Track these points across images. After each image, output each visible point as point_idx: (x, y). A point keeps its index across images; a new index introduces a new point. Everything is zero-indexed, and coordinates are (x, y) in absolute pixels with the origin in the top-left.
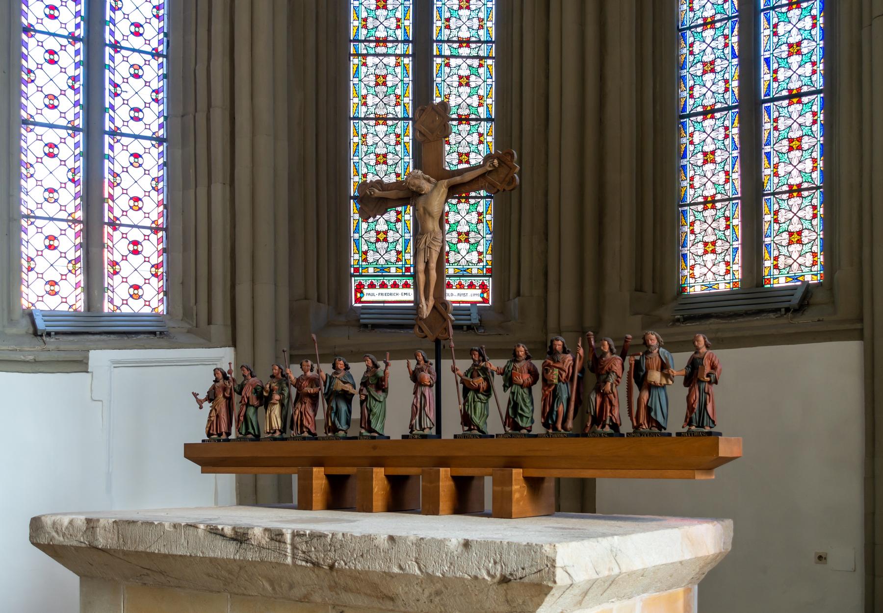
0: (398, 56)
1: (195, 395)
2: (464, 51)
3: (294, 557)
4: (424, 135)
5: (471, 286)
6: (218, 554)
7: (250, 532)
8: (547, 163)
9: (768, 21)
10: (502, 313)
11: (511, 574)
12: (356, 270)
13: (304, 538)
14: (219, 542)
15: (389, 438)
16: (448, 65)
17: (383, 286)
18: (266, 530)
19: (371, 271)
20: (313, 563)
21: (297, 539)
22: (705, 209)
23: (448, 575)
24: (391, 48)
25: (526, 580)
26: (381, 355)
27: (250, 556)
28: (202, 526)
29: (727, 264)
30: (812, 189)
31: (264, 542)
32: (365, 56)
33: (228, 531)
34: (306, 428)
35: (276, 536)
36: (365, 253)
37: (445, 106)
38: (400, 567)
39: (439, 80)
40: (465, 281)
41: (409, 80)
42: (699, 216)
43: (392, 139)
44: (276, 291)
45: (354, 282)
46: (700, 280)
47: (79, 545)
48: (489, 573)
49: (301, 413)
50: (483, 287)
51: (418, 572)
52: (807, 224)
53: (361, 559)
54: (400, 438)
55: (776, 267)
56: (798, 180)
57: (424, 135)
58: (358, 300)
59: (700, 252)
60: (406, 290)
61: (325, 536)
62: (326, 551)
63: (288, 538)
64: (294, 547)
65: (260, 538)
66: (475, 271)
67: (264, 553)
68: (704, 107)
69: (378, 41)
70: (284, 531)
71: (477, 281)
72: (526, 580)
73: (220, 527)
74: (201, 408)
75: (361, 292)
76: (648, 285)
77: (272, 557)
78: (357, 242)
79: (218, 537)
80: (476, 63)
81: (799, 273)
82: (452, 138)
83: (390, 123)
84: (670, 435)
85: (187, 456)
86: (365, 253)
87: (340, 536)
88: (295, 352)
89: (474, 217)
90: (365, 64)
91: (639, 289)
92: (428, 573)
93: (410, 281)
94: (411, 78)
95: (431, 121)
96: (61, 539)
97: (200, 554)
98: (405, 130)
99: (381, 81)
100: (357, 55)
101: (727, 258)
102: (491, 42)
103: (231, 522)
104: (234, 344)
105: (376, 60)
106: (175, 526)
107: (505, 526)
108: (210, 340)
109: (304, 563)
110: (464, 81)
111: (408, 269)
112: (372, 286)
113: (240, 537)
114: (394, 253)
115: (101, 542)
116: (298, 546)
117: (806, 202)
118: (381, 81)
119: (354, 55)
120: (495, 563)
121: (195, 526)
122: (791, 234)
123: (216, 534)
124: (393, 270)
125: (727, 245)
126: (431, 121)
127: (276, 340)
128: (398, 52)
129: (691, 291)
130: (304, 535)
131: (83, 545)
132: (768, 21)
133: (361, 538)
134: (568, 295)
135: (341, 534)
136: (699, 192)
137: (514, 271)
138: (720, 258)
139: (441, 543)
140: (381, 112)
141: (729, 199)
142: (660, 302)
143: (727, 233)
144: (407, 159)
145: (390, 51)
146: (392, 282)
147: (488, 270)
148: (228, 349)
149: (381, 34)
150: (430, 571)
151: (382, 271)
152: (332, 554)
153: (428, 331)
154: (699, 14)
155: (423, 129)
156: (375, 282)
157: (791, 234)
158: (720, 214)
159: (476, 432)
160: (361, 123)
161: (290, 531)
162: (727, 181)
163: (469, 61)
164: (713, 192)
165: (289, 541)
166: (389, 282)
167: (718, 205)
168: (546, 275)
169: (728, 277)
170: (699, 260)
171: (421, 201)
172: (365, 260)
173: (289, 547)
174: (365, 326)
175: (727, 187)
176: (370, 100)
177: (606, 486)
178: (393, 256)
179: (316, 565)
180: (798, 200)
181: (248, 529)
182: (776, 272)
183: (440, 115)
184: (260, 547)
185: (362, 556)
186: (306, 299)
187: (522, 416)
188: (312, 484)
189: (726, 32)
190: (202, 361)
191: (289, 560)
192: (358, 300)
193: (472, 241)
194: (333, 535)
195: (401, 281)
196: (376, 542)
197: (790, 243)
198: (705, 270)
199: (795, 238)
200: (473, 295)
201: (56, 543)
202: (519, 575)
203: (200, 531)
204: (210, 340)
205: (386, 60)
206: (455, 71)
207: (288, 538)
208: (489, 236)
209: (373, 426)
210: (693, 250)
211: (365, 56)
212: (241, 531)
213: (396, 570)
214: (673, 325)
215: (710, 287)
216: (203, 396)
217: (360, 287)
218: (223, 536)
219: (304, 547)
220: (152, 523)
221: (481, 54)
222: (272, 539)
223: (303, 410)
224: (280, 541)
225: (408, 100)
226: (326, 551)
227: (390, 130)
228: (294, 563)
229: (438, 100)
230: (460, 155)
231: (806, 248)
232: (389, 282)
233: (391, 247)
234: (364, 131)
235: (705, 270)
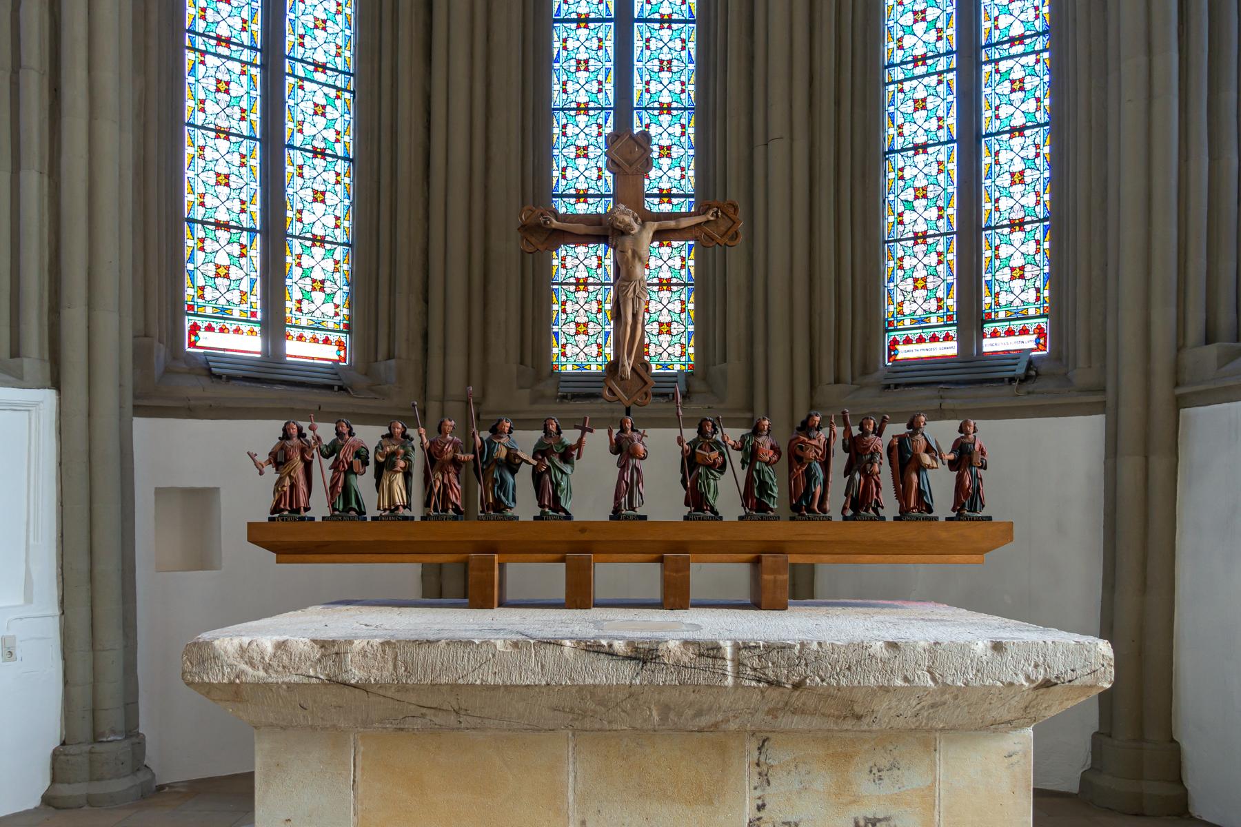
0: (244, 63)
1: (252, 456)
2: (319, 76)
3: (738, 675)
4: (618, 165)
5: (326, 341)
6: (601, 679)
7: (660, 647)
8: (427, 217)
9: (641, 119)
10: (366, 374)
11: (1057, 678)
12: (191, 307)
13: (757, 652)
14: (604, 663)
15: (645, 518)
16: (301, 87)
17: (921, 340)
18: (686, 643)
19: (209, 311)
20: (768, 682)
21: (745, 653)
22: (577, 290)
23: (973, 683)
24: (234, 51)
25: (1077, 683)
26: (305, 414)
27: (660, 679)
28: (568, 643)
29: (599, 346)
30: (567, 284)
31: (686, 659)
32: (203, 53)
33: (619, 646)
34: (453, 503)
35: (711, 651)
36: (202, 288)
37: (646, 136)
38: (906, 679)
39: (291, 102)
40: (321, 335)
41: (256, 93)
42: (571, 297)
43: (236, 159)
44: (120, 322)
45: (188, 322)
46: (571, 359)
47: (305, 681)
48: (1028, 678)
49: (444, 485)
50: (340, 344)
51: (931, 683)
52: (676, 317)
53: (847, 672)
54: (682, 519)
55: (564, 354)
56: (668, 275)
57: (618, 165)
58: (192, 344)
59: (573, 331)
60: (1025, 338)
61: (791, 647)
62: (791, 666)
63: (728, 652)
64: (738, 663)
65: (679, 654)
66: (331, 326)
67: (686, 674)
68: (577, 190)
69: (219, 39)
70: (721, 643)
71: (333, 337)
72: (1077, 683)
73: (604, 642)
74: (261, 473)
75: (196, 335)
76: (528, 360)
77: (700, 678)
78: (191, 274)
79: (602, 656)
80: (333, 93)
81: (669, 362)
82: (653, 173)
83: (233, 139)
84: (936, 519)
85: (252, 539)
86: (202, 288)
87: (815, 646)
88: (139, 402)
89: (329, 265)
90: (203, 63)
91: (522, 363)
92: (944, 684)
93: (257, 328)
94: (259, 92)
95: (629, 154)
96: (262, 673)
97: (566, 681)
98: (251, 152)
99: (222, 87)
100: (989, 62)
101: (599, 341)
102: (349, 74)
103: (629, 634)
104: (56, 383)
105: (217, 61)
106: (515, 645)
107: (894, 619)
108: (21, 378)
109: (754, 683)
110: (319, 110)
111: (254, 314)
112: (210, 328)
113: (644, 655)
114: (237, 293)
115: (355, 675)
116: (746, 661)
117: (675, 296)
118: (222, 87)
119: (188, 48)
120: (1036, 666)
121: (557, 643)
122: (661, 324)
123: (598, 652)
124: (236, 314)
125: (599, 329)
126: (629, 154)
127: (120, 385)
128: (244, 58)
129: (563, 370)
130: (757, 647)
131: (314, 681)
132: (641, 119)
133: (847, 647)
134: (457, 361)
135: (815, 643)
136: (571, 272)
137: (383, 330)
138: (592, 340)
139: (964, 649)
140: (224, 124)
141: (602, 284)
142: (538, 378)
143: (599, 316)
144: (253, 185)
145: (235, 55)
146: (206, 324)
147: (346, 326)
148: (47, 391)
149: (224, 31)
150: (949, 682)
151: (920, 322)
152: (801, 669)
153: (627, 391)
154: (572, 97)
155: (617, 158)
156: (214, 325)
157: (661, 324)
158: (592, 297)
159: (709, 514)
160: (199, 132)
161: (729, 643)
162: (599, 266)
163: (326, 89)
164: (585, 274)
165: (729, 656)
166: (216, 324)
167: (591, 288)
168: (426, 337)
169: (599, 359)
170: (571, 340)
171: (628, 242)
172: (202, 297)
173: (729, 663)
174: (219, 377)
175: (599, 271)
176: (209, 106)
177: (828, 570)
178: (235, 296)
179: (775, 684)
180: (667, 294)
181: (658, 643)
182: (564, 359)
183: (640, 146)
184: (679, 666)
185: (849, 669)
186: (146, 336)
187: (770, 496)
188: (689, 577)
189: (600, 121)
190: (12, 404)
191: (730, 681)
192: (192, 344)
193: (328, 291)
194: (802, 644)
195: (245, 327)
196: (871, 651)
197: (660, 333)
198: (577, 350)
199: (665, 329)
200: (330, 353)
201: (249, 679)
202: (1068, 677)
203: (566, 650)
204: (21, 378)
205: (230, 64)
206: (309, 96)
207: (728, 652)
208: (346, 289)
209: (563, 504)
210: (565, 329)
211: (997, 62)
212: (646, 646)
213: (899, 682)
214: (561, 402)
215: (581, 367)
216: (263, 457)
217: (195, 329)
218: (611, 654)
219: (756, 663)
220: (470, 643)
221: (339, 84)
222: (701, 655)
223: (446, 481)
224: (714, 657)
225: (256, 117)
226: (791, 666)
227: (234, 147)
228: (737, 686)
229: (636, 130)
230: (315, 192)
231: (676, 339)
232: (232, 326)
233: (233, 285)
234: (202, 143)
235: (577, 350)
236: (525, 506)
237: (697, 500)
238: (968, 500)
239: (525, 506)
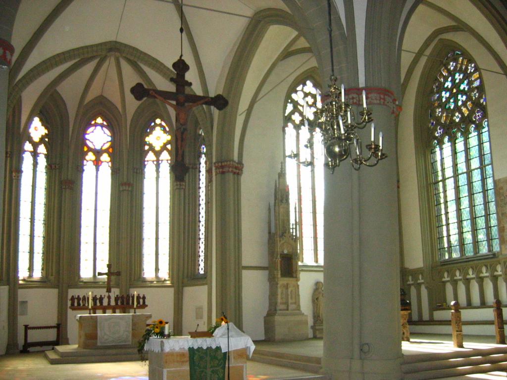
104: (8, 284)
236: (98, 304)
237: (117, 303)
238: (144, 302)
239: (98, 304)
